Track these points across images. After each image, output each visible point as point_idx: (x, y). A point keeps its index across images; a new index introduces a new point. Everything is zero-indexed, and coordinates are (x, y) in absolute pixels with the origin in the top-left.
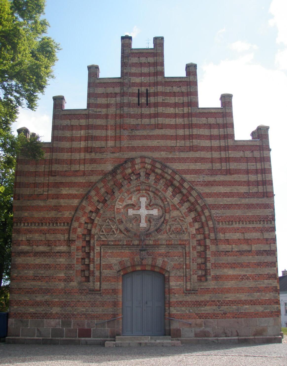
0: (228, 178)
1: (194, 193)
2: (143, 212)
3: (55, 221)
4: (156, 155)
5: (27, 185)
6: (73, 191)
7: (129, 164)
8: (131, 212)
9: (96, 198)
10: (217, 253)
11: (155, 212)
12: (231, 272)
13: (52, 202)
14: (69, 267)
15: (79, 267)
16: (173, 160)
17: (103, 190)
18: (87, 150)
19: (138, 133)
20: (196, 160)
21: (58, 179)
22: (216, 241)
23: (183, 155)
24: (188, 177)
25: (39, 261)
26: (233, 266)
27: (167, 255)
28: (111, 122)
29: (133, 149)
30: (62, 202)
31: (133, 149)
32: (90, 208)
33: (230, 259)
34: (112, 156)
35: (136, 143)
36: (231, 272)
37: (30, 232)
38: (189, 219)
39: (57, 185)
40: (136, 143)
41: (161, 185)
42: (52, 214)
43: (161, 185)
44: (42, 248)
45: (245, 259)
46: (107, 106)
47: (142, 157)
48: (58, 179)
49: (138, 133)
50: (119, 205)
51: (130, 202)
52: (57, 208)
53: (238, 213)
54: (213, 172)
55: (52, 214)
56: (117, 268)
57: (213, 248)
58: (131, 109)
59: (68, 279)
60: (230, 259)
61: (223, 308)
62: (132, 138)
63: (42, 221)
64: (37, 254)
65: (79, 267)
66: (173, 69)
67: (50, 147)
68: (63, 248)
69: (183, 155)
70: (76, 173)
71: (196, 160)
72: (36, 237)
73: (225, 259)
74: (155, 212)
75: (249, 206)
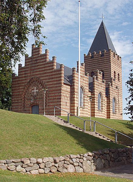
0: (52, 80)
1: (45, 85)
2: (35, 91)
3: (19, 95)
4: (38, 76)
5: (14, 87)
6: (22, 87)
7: (32, 80)
8: (33, 91)
9: (26, 89)
10: (49, 100)
11: (37, 91)
12: (51, 104)
13: (18, 91)
14: (21, 105)
15: (23, 105)
16: (41, 77)
17: (27, 86)
18: (25, 77)
19: (34, 71)
20: (46, 76)
21: (19, 85)
22: (49, 97)
23: (43, 75)
24: (44, 81)
25: (16, 104)
26: (52, 103)
27: (39, 101)
28: (29, 69)
29: (33, 75)
30: (20, 90)
31: (33, 75)
32: (25, 91)
33: (51, 101)
34: (29, 78)
35: (34, 74)
36: (51, 104)
37: (14, 98)
38: (40, 85)
39: (19, 86)
40: (34, 74)
41: (38, 84)
42: (18, 93)
43: (38, 84)
44: (17, 101)
45: (55, 100)
46: (29, 65)
47: (35, 77)
48: (19, 85)
49: (34, 71)
50: (30, 90)
51: (32, 89)
52: (19, 92)
53: (54, 89)
54: (49, 79)
55: (18, 93)
56: (30, 105)
57: (48, 98)
58: (33, 65)
59: (21, 108)
60: (51, 101)
61: (49, 113)
62: (33, 72)
63: (17, 95)
64: (16, 103)
65: (23, 105)
66: (43, 52)
67: (17, 77)
68: (20, 101)
69: (43, 75)
70: (23, 83)
71: (46, 76)
72: (15, 99)
73: (50, 101)
74: (37, 91)
75: (56, 87)
